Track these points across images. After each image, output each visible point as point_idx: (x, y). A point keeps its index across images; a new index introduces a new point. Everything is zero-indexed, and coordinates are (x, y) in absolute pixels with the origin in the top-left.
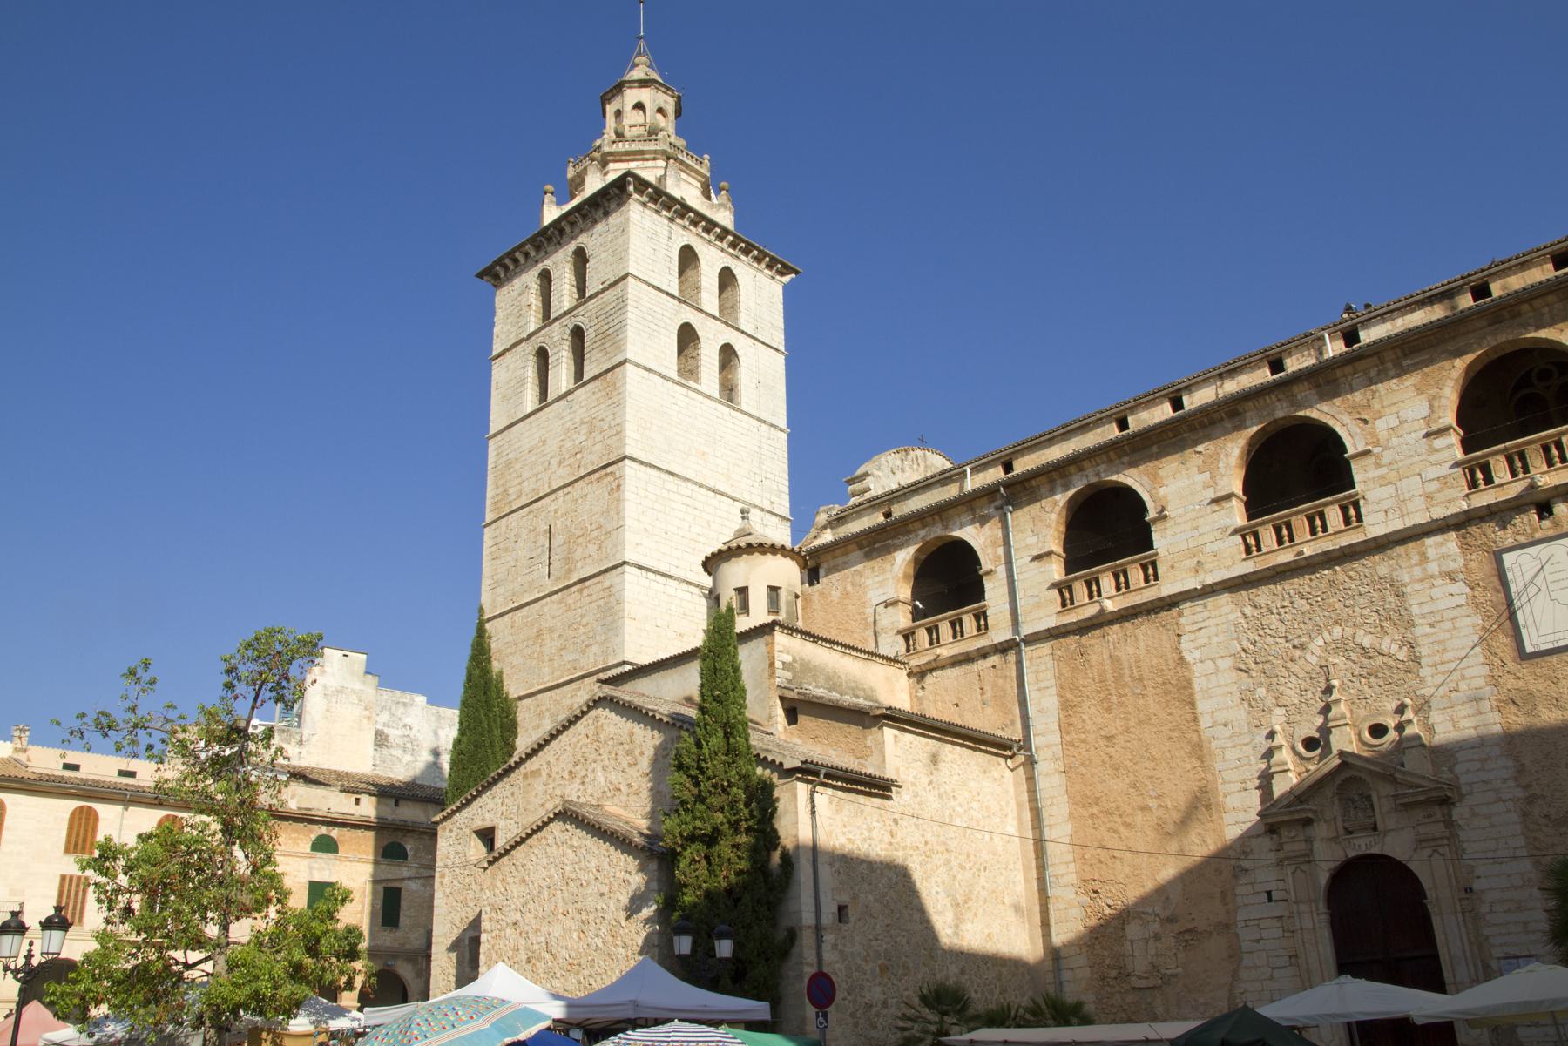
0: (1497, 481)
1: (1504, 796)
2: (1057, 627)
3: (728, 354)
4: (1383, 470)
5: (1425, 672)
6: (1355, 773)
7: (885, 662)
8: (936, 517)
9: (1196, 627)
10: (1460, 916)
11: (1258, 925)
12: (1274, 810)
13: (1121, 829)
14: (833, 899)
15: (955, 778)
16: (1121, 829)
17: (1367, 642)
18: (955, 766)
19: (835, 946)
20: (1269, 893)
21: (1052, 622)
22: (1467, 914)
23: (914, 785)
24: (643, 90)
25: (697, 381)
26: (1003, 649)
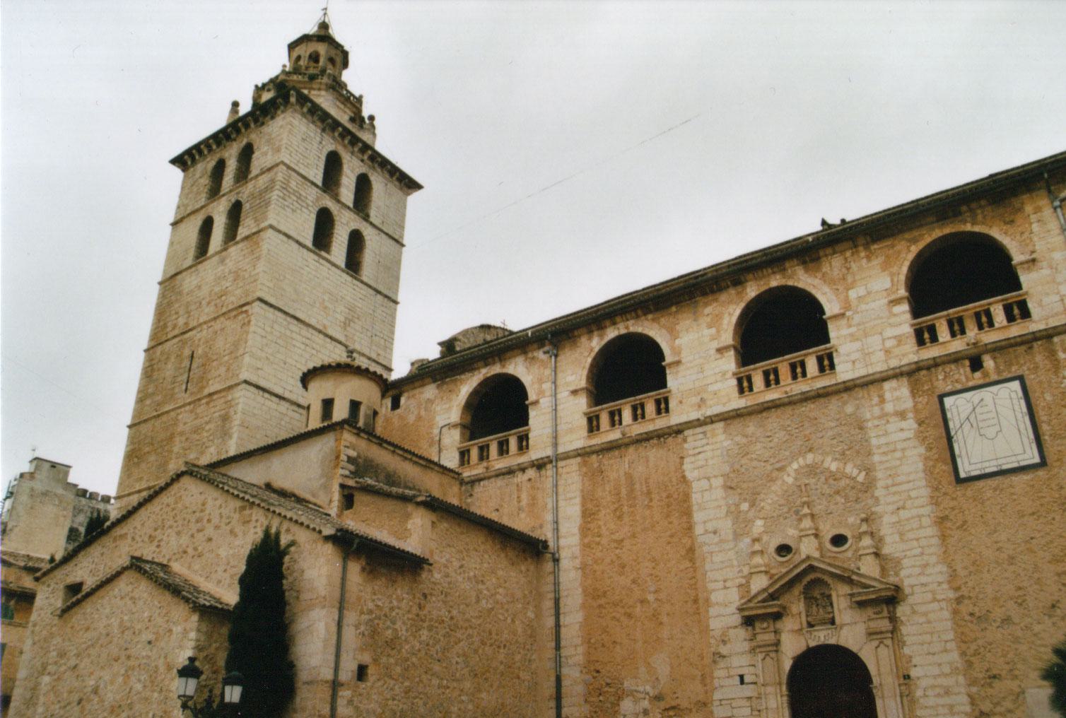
0: (941, 340)
1: (938, 597)
2: (584, 448)
3: (356, 241)
4: (853, 330)
5: (879, 493)
6: (819, 575)
7: (441, 470)
8: (497, 358)
9: (697, 451)
10: (898, 699)
11: (731, 704)
12: (752, 605)
13: (622, 618)
14: (354, 659)
15: (485, 565)
16: (622, 618)
17: (834, 467)
18: (486, 556)
19: (350, 702)
20: (742, 677)
21: (579, 444)
22: (905, 698)
23: (446, 566)
24: (321, 44)
25: (328, 252)
26: (540, 465)
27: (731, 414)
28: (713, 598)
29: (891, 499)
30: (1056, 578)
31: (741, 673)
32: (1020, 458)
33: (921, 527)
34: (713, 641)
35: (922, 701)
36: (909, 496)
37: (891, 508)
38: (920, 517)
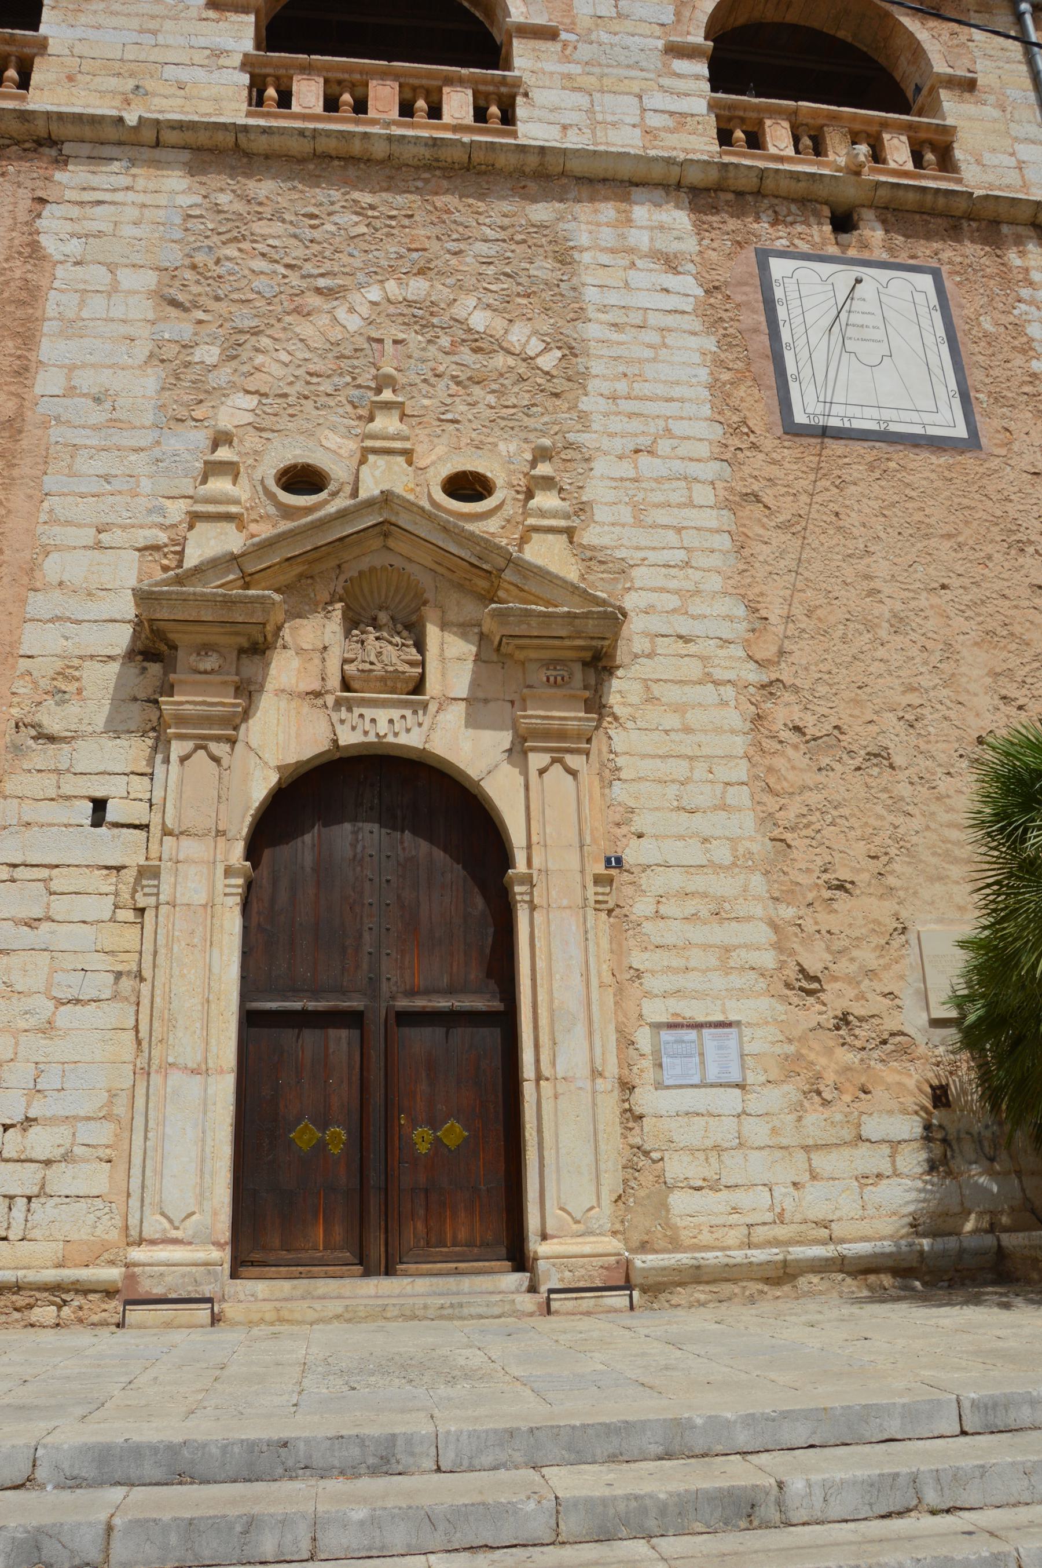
1: (719, 674)
9: (88, 196)
17: (479, 320)
20: (99, 805)
27: (220, 136)
28: (52, 567)
29: (617, 424)
30: (989, 680)
31: (99, 794)
32: (927, 418)
33: (690, 504)
34: (23, 688)
35: (648, 927)
36: (668, 430)
37: (618, 445)
38: (690, 480)
